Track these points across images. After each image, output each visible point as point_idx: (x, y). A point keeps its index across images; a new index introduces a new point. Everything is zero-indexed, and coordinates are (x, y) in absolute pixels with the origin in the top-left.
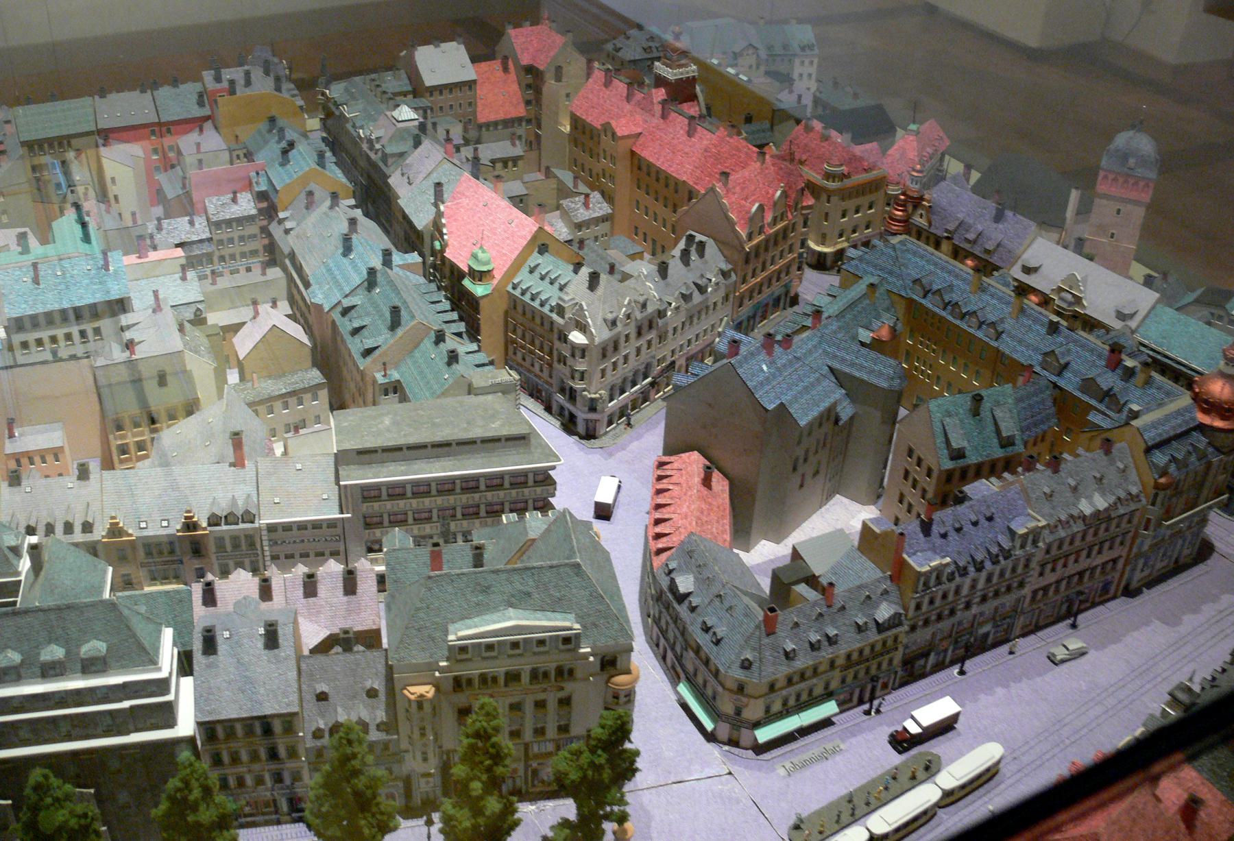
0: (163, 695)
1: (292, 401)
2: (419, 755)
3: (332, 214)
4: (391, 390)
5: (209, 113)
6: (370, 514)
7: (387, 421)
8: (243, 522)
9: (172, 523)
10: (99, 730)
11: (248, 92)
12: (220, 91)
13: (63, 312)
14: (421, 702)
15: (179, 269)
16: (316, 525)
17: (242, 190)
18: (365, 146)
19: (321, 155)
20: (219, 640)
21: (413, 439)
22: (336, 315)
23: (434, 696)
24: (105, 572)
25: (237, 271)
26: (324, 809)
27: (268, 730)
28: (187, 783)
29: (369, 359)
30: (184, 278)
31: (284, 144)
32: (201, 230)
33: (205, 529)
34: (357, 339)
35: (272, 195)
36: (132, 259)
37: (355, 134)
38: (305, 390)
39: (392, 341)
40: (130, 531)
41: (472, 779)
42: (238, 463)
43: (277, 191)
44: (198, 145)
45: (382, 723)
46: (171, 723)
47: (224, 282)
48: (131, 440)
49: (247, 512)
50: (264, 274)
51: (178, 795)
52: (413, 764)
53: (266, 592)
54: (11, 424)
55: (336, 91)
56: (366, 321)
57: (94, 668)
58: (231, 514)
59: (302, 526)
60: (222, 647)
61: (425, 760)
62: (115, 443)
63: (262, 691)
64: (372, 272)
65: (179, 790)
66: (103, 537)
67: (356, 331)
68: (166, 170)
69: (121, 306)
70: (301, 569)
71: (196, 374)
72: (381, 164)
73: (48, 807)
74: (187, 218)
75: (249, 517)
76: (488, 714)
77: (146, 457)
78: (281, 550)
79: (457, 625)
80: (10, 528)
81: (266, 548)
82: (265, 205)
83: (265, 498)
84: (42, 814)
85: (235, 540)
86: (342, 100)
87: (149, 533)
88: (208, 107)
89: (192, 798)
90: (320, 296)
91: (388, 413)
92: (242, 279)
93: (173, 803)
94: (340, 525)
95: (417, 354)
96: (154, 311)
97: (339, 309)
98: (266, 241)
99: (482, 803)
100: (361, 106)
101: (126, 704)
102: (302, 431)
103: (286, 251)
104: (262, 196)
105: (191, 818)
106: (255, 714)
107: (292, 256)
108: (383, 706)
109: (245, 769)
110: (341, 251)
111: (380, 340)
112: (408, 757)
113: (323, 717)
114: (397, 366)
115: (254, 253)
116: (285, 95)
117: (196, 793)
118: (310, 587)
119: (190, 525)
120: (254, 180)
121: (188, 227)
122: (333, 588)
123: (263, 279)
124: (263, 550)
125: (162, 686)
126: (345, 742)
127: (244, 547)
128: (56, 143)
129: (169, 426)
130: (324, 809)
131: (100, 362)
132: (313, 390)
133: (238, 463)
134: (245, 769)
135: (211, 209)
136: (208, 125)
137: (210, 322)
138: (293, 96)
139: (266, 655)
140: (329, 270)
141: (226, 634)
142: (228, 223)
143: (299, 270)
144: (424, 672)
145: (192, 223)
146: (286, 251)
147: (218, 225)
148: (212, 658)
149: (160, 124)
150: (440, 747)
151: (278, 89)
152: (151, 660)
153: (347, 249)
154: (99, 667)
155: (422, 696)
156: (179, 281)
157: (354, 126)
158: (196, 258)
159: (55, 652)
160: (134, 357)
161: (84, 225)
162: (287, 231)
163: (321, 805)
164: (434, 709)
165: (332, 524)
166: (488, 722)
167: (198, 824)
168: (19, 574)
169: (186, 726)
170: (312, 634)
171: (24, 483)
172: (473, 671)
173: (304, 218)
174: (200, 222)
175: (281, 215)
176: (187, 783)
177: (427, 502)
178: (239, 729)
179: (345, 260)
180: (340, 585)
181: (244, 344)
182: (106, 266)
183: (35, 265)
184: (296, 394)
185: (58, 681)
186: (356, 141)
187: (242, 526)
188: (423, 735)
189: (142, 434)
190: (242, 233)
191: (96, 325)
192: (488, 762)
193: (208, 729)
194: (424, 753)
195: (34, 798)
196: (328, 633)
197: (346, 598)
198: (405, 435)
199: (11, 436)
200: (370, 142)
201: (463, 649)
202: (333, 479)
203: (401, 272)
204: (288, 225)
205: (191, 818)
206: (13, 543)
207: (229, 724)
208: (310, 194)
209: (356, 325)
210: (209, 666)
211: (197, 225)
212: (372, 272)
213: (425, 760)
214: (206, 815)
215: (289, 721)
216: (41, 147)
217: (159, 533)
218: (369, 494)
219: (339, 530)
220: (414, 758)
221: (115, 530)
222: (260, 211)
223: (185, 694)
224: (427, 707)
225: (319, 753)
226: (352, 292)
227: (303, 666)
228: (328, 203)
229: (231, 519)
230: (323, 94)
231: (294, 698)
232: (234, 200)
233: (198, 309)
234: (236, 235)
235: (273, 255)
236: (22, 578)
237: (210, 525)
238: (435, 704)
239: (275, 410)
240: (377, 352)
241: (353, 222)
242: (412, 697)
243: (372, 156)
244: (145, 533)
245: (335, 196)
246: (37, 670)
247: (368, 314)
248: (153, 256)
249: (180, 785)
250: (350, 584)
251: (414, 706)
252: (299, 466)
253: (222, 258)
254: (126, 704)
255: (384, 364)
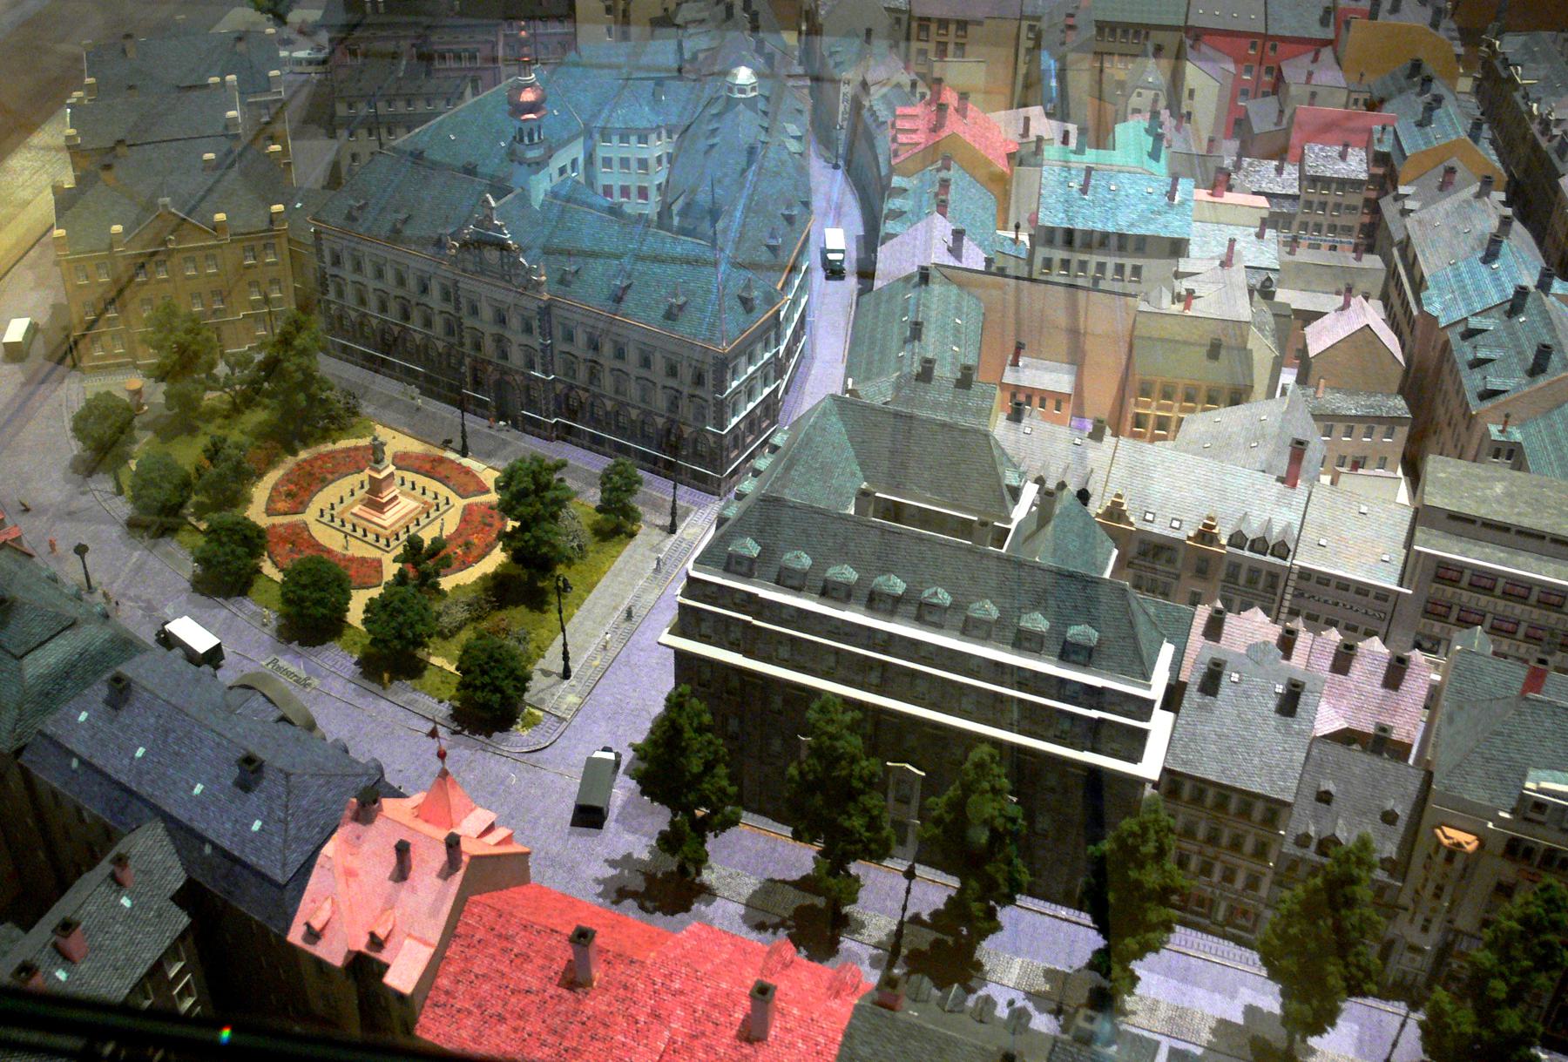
0: (1142, 720)
1: (1360, 428)
2: (1419, 920)
3: (1478, 204)
4: (1505, 452)
5: (1331, 36)
6: (1438, 601)
7: (1499, 488)
8: (1272, 554)
9: (1185, 526)
10: (1051, 733)
11: (1393, 20)
12: (1355, 11)
13: (1105, 236)
14: (1454, 850)
15: (1258, 223)
16: (1363, 589)
17: (1185, 176)
18: (1535, 128)
19: (1477, 126)
20: (1225, 681)
21: (1527, 522)
22: (1454, 337)
23: (1474, 853)
24: (1110, 553)
25: (1318, 247)
26: (1292, 931)
27: (1245, 812)
28: (1144, 828)
29: (1488, 404)
30: (1260, 236)
31: (1427, 97)
32: (1289, 181)
33: (1223, 547)
34: (1477, 374)
35: (1395, 159)
36: (1203, 194)
37: (1524, 108)
38: (1380, 420)
39: (1527, 389)
40: (1132, 519)
41: (1493, 976)
42: (1289, 480)
43: (1405, 157)
44: (1310, 74)
45: (1389, 859)
46: (1135, 758)
47: (1304, 255)
48: (1153, 412)
49: (1283, 544)
50: (1358, 259)
51: (1130, 841)
52: (1406, 929)
53: (1287, 643)
54: (1019, 349)
55: (1508, 45)
56: (1495, 354)
57: (1074, 657)
58: (1263, 540)
59: (1344, 584)
60: (1225, 690)
61: (1425, 929)
62: (1133, 409)
63: (1256, 761)
64: (1522, 292)
65: (1132, 834)
66: (1098, 515)
67: (1478, 363)
68: (1255, 97)
69: (1177, 248)
70: (1334, 636)
71: (1256, 356)
72: (1554, 157)
73: (983, 792)
74: (1275, 163)
75: (1282, 550)
76: (1550, 901)
77: (1164, 438)
78: (1309, 606)
79: (1541, 774)
80: (1015, 466)
81: (1288, 597)
82: (1380, 171)
83: (1309, 534)
84: (974, 797)
85: (1254, 571)
86: (1517, 59)
87: (1156, 529)
88: (1332, 27)
89: (1143, 849)
90: (1437, 304)
91: (1503, 479)
92: (1322, 257)
93: (1120, 848)
94: (1392, 598)
95: (1556, 417)
96: (1223, 264)
97: (1461, 328)
98: (1366, 219)
99: (1496, 1012)
100: (1542, 73)
101: (1095, 714)
102: (1360, 471)
103: (1398, 236)
104: (1381, 159)
105: (1133, 874)
106: (1238, 785)
107: (1405, 246)
108: (1397, 838)
109: (1195, 848)
110: (1480, 254)
111: (1509, 384)
112: (1404, 917)
113: (1317, 822)
114: (1522, 425)
115: (1347, 230)
116: (1442, 34)
117: (1150, 848)
118: (1343, 661)
119: (1206, 534)
120: (1376, 136)
121: (1273, 174)
122: (1371, 673)
123: (1355, 264)
124: (1282, 598)
125: (1143, 708)
126: (1353, 858)
127: (1261, 585)
128: (1119, 31)
129: (1204, 410)
130: (1292, 931)
131: (1144, 307)
132: (1392, 422)
133: (1289, 480)
134: (1195, 848)
135: (1310, 160)
136: (1327, 54)
137: (1277, 299)
138: (1452, 39)
139: (1274, 719)
140: (1458, 275)
141: (1235, 677)
142: (1326, 182)
143: (1411, 265)
144: (1469, 816)
145: (1279, 170)
146: (1398, 236)
147: (1315, 180)
148: (1208, 699)
149: (1266, 37)
150: (1450, 922)
151: (1435, 25)
152: (1144, 674)
153: (1490, 256)
154: (1081, 658)
155: (1459, 845)
156: (1253, 238)
157: (1526, 97)
158: (1279, 218)
159: (1038, 622)
160: (1188, 313)
161: (1281, 112)
162: (1405, 213)
163: (1289, 925)
164: (1465, 869)
165: (1383, 595)
166: (1547, 911)
167: (1138, 885)
168: (1009, 521)
169: (1150, 767)
170: (1328, 718)
171: (1025, 421)
172: (1543, 839)
173: (1434, 201)
174: (1291, 172)
175: (1402, 190)
176: (1144, 828)
177: (1518, 610)
178: (1211, 793)
179: (1484, 271)
180: (1382, 672)
181: (1319, 339)
182: (1171, 195)
183: (1089, 171)
184: (1371, 422)
185: (1030, 657)
186: (1522, 118)
187: (1269, 558)
188: (1437, 896)
189: (1169, 408)
190: (1340, 200)
191: (1138, 262)
192: (1527, 963)
193: (1172, 780)
194: (1428, 921)
195: (972, 775)
196: (1346, 726)
197: (1382, 691)
198: (1519, 514)
199: (1015, 363)
200: (1546, 124)
201: (1539, 806)
202: (1403, 536)
203: (1557, 304)
204: (1409, 205)
205: (1133, 874)
206: (1015, 483)
207: (1201, 785)
208: (1451, 171)
209: (1481, 355)
210: (1201, 707)
211: (1285, 175)
212: (1522, 292)
213: (1425, 929)
214: (1151, 878)
215: (1275, 810)
216: (1125, 32)
217: (1165, 533)
218: (1445, 573)
219: (1388, 606)
220: (1411, 921)
221: (1115, 512)
222: (1372, 176)
223: (1160, 725)
224: (1458, 863)
225: (1294, 864)
226: (1485, 312)
227: (1315, 752)
228: (1475, 188)
229: (1258, 546)
230: (1490, 45)
231: (1293, 784)
232: (1343, 156)
233: (1269, 279)
234: (1331, 200)
235: (1372, 237)
236: (1013, 527)
237: (1230, 544)
238: (1472, 860)
239: (1334, 433)
240: (1502, 398)
241: (1505, 222)
242: (1446, 842)
243: (1544, 143)
244: (1148, 528)
245: (1487, 183)
246: (1010, 635)
247: (1500, 346)
248: (1229, 197)
249: (1136, 828)
250: (1395, 674)
251: (1443, 854)
252: (1364, 509)
253: (1304, 226)
254: (1095, 714)
255: (1507, 416)
